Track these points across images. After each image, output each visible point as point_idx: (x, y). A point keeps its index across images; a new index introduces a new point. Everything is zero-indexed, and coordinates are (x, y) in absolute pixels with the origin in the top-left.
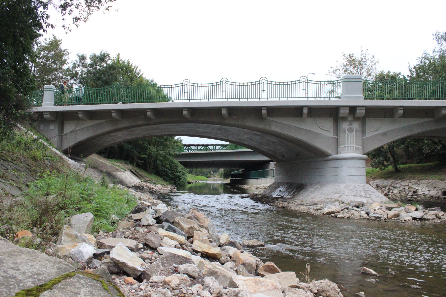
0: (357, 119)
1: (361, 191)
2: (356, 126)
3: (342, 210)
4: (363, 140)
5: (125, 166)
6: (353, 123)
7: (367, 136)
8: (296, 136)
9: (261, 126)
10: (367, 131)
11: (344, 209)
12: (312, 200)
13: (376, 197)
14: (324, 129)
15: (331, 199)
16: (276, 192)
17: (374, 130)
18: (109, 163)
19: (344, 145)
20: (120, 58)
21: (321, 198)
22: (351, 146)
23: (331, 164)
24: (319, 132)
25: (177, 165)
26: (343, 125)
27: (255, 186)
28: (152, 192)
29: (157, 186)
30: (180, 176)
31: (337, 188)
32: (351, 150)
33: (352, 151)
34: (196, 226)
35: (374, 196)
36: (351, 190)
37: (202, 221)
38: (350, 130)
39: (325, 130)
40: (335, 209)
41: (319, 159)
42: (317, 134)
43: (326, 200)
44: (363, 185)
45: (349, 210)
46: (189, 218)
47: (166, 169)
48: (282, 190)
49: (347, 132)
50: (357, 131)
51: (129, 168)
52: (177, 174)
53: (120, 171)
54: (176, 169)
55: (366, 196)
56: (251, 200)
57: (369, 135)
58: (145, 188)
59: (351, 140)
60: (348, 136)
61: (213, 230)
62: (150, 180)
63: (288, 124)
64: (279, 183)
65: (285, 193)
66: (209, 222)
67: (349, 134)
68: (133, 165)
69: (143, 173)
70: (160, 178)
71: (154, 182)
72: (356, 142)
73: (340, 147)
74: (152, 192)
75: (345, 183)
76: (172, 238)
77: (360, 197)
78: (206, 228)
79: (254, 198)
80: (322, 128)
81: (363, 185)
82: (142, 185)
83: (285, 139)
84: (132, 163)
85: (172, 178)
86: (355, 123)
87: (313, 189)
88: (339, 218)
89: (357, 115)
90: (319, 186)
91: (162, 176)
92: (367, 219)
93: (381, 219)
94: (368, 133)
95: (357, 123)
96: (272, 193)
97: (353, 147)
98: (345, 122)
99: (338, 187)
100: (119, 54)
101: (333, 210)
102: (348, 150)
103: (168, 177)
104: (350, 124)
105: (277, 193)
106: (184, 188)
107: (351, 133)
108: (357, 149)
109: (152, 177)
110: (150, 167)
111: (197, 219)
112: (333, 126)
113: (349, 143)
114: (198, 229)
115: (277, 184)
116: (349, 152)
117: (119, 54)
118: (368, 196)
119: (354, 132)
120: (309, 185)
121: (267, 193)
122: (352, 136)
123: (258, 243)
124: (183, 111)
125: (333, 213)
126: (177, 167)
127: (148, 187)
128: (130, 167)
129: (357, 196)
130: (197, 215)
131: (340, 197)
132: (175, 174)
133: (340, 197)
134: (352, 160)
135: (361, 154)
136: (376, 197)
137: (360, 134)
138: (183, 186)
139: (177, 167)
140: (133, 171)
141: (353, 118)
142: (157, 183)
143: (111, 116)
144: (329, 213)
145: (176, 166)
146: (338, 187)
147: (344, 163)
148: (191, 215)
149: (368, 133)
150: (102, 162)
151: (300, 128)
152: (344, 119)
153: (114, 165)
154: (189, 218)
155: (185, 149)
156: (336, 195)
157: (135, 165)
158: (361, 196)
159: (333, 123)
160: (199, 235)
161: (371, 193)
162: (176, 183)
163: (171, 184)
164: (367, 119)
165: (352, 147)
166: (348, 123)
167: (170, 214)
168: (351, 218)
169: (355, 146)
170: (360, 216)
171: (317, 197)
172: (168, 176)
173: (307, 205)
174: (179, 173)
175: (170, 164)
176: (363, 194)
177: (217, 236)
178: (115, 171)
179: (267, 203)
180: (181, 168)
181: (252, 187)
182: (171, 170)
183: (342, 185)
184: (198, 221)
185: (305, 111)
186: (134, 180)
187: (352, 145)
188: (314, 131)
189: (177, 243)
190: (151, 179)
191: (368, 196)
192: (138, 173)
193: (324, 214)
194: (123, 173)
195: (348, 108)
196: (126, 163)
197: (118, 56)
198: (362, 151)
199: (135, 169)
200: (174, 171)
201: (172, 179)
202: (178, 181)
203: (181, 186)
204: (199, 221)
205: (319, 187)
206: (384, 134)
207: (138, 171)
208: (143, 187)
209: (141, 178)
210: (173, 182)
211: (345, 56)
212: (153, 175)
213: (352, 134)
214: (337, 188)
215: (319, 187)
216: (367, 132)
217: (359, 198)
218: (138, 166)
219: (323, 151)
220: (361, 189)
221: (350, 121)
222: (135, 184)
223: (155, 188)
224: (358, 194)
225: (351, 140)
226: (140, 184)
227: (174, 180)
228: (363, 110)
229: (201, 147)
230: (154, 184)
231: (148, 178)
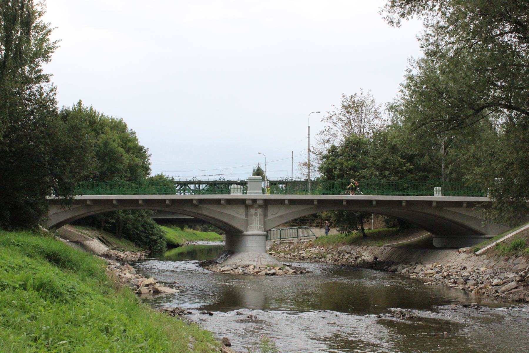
0: (260, 206)
2: (260, 211)
4: (265, 222)
5: (93, 234)
9: (195, 211)
18: (76, 231)
20: (82, 106)
24: (235, 215)
28: (118, 259)
29: (126, 253)
38: (256, 214)
42: (234, 217)
49: (253, 216)
50: (260, 215)
51: (97, 235)
53: (89, 240)
54: (152, 231)
58: (113, 255)
62: (118, 247)
67: (255, 217)
68: (101, 231)
69: (112, 239)
70: (132, 243)
71: (123, 249)
74: (118, 259)
82: (110, 253)
84: (99, 227)
85: (146, 242)
100: (80, 101)
104: (256, 210)
108: (260, 228)
109: (120, 243)
110: (119, 229)
117: (80, 101)
118: (259, 261)
125: (224, 271)
126: (153, 228)
127: (116, 255)
128: (97, 233)
132: (150, 237)
137: (262, 217)
139: (153, 228)
140: (100, 238)
143: (86, 203)
145: (151, 228)
150: (70, 231)
151: (223, 213)
152: (251, 206)
153: (81, 233)
155: (179, 189)
157: (102, 228)
158: (254, 261)
161: (262, 259)
162: (152, 248)
163: (145, 249)
166: (254, 209)
169: (258, 225)
172: (141, 240)
174: (155, 236)
175: (143, 226)
178: (84, 240)
182: (146, 233)
186: (102, 248)
187: (257, 225)
191: (259, 261)
192: (105, 240)
194: (92, 242)
196: (93, 230)
197: (80, 103)
199: (103, 235)
200: (149, 233)
202: (153, 246)
203: (158, 252)
206: (281, 217)
207: (106, 237)
208: (111, 255)
209: (109, 245)
210: (147, 247)
211: (345, 97)
212: (123, 239)
216: (269, 216)
218: (106, 230)
220: (257, 256)
222: (103, 252)
223: (122, 255)
224: (252, 260)
226: (108, 252)
227: (149, 245)
229: (204, 185)
230: (123, 250)
231: (116, 244)
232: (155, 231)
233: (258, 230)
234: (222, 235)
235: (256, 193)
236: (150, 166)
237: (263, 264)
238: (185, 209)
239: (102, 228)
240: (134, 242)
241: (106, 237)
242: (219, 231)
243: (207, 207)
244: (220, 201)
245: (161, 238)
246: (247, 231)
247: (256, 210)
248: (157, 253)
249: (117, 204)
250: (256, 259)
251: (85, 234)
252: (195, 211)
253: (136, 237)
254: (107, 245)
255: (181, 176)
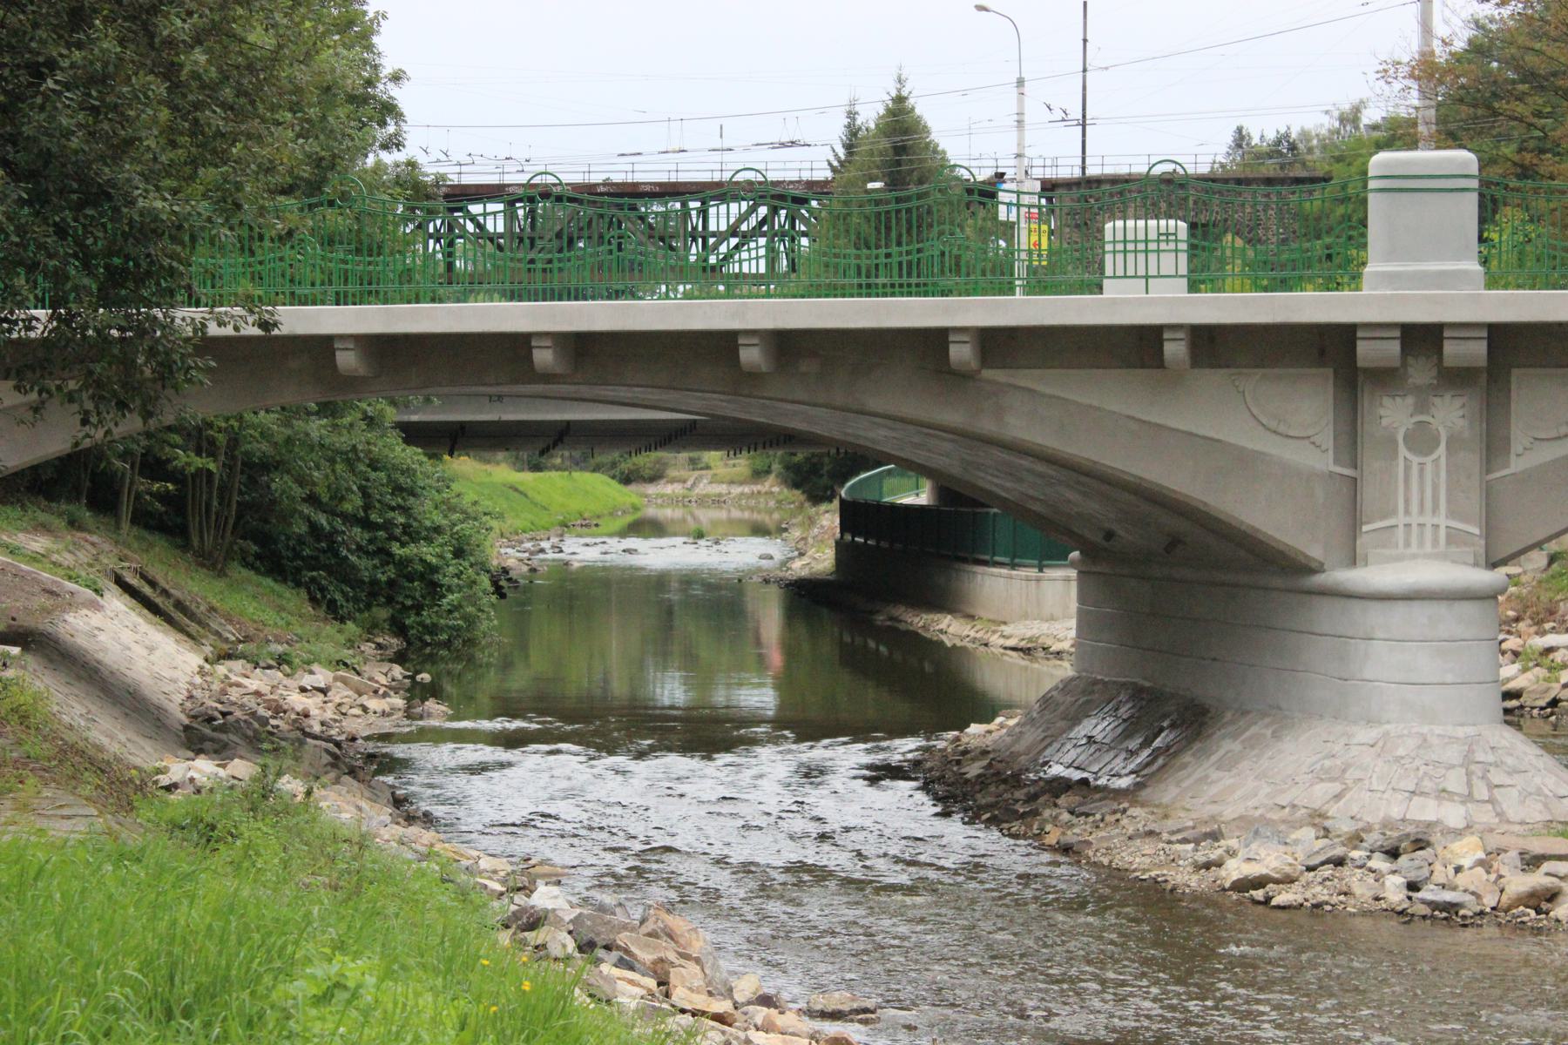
0: (1456, 378)
1: (1452, 767)
3: (1310, 869)
4: (1489, 493)
6: (1437, 401)
7: (1517, 465)
8: (1134, 471)
9: (952, 416)
10: (1519, 436)
11: (1323, 864)
12: (1214, 809)
13: (1525, 796)
14: (1282, 428)
15: (1294, 806)
16: (1069, 746)
17: (1553, 434)
19: (1384, 517)
21: (1250, 804)
22: (1421, 525)
23: (1326, 615)
25: (403, 480)
26: (1382, 412)
27: (1018, 632)
30: (434, 569)
31: (1337, 748)
32: (1421, 544)
33: (1428, 548)
34: (672, 956)
35: (1514, 792)
36: (1398, 759)
37: (682, 941)
38: (1421, 441)
39: (1287, 436)
40: (1275, 864)
41: (1277, 582)
42: (1245, 460)
43: (1269, 816)
44: (1470, 730)
45: (1346, 871)
46: (650, 935)
47: (322, 520)
48: (1099, 738)
49: (1403, 451)
50: (1454, 443)
52: (410, 551)
53: (72, 604)
54: (405, 510)
55: (1470, 794)
56: (921, 797)
57: (1525, 456)
59: (1422, 491)
60: (1407, 469)
61: (715, 967)
62: (247, 639)
63: (1095, 403)
64: (1095, 682)
65: (1112, 754)
66: (701, 943)
67: (1415, 460)
69: (193, 585)
71: (279, 648)
72: (1449, 501)
73: (1365, 528)
75: (1380, 723)
76: (631, 982)
77: (1437, 798)
78: (697, 961)
79: (941, 779)
80: (1273, 424)
81: (1470, 730)
83: (1087, 474)
85: (374, 582)
86: (1448, 397)
87: (1236, 746)
88: (1278, 907)
89: (1449, 361)
90: (1267, 726)
91: (298, 570)
92: (1402, 913)
93: (1462, 912)
94: (1520, 450)
95: (1458, 402)
96: (1047, 752)
97: (1436, 527)
98: (1393, 397)
99: (1343, 741)
101: (1264, 871)
102: (1407, 544)
103: (345, 580)
104: (1422, 407)
105: (1073, 754)
106: (471, 659)
107: (1426, 455)
108: (1453, 538)
111: (671, 936)
112: (1331, 416)
113: (1415, 508)
114: (677, 962)
115: (1084, 692)
116: (1414, 557)
118: (1482, 792)
119: (1442, 450)
120: (1229, 715)
121: (1020, 747)
122: (1429, 469)
123: (855, 1006)
124: (530, 349)
125: (1259, 882)
129: (1422, 794)
130: (670, 924)
131: (1338, 797)
132: (396, 549)
133: (1338, 797)
134: (1416, 604)
135: (1476, 565)
136: (1525, 796)
137: (1471, 460)
138: (458, 643)
141: (1434, 372)
142: (299, 652)
144: (1243, 885)
145: (398, 489)
146: (1343, 741)
147: (1375, 617)
148: (655, 927)
149: (1520, 450)
152: (1386, 378)
154: (650, 935)
156: (1323, 785)
157: (126, 511)
158: (1443, 794)
159: (1335, 399)
160: (683, 976)
161: (1497, 777)
162: (410, 620)
164: (1515, 372)
165: (1428, 532)
166: (1410, 400)
167: (589, 923)
168: (1328, 908)
169: (1443, 521)
170: (1377, 899)
171: (1238, 794)
172: (344, 574)
173: (1174, 838)
174: (429, 540)
176: (1455, 781)
177: (725, 983)
179: (998, 817)
180: (410, 455)
181: (995, 640)
182: (367, 524)
183: (1364, 734)
184: (673, 944)
185: (1175, 349)
187: (1428, 520)
188: (1232, 440)
189: (644, 992)
190: (252, 631)
191: (1482, 792)
193: (1224, 890)
194: (96, 619)
195: (1397, 333)
198: (1482, 551)
200: (388, 525)
201: (373, 595)
202: (418, 608)
203: (447, 644)
204: (676, 942)
205: (1269, 732)
209: (193, 627)
210: (383, 613)
212: (238, 572)
213: (1428, 460)
214: (1337, 748)
215: (1269, 732)
216: (1516, 447)
217: (1432, 803)
218: (144, 520)
219: (1281, 548)
220: (1453, 754)
221: (1418, 390)
224: (1427, 785)
225: (1422, 491)
227: (390, 601)
228: (1479, 342)
230: (282, 660)
232: (428, 512)
233: (1443, 557)
234: (633, 487)
235: (1442, 279)
236: (400, 95)
237: (1512, 814)
238: (875, 403)
239: (126, 511)
240: (298, 584)
241: (156, 572)
242: (614, 465)
243: (1041, 388)
244: (1160, 342)
245: (459, 553)
246: (1353, 561)
247: (1422, 407)
248: (444, 653)
249: (362, 371)
250: (1455, 781)
251: (35, 558)
252: (952, 416)
253: (307, 552)
254: (181, 629)
255: (520, 155)
